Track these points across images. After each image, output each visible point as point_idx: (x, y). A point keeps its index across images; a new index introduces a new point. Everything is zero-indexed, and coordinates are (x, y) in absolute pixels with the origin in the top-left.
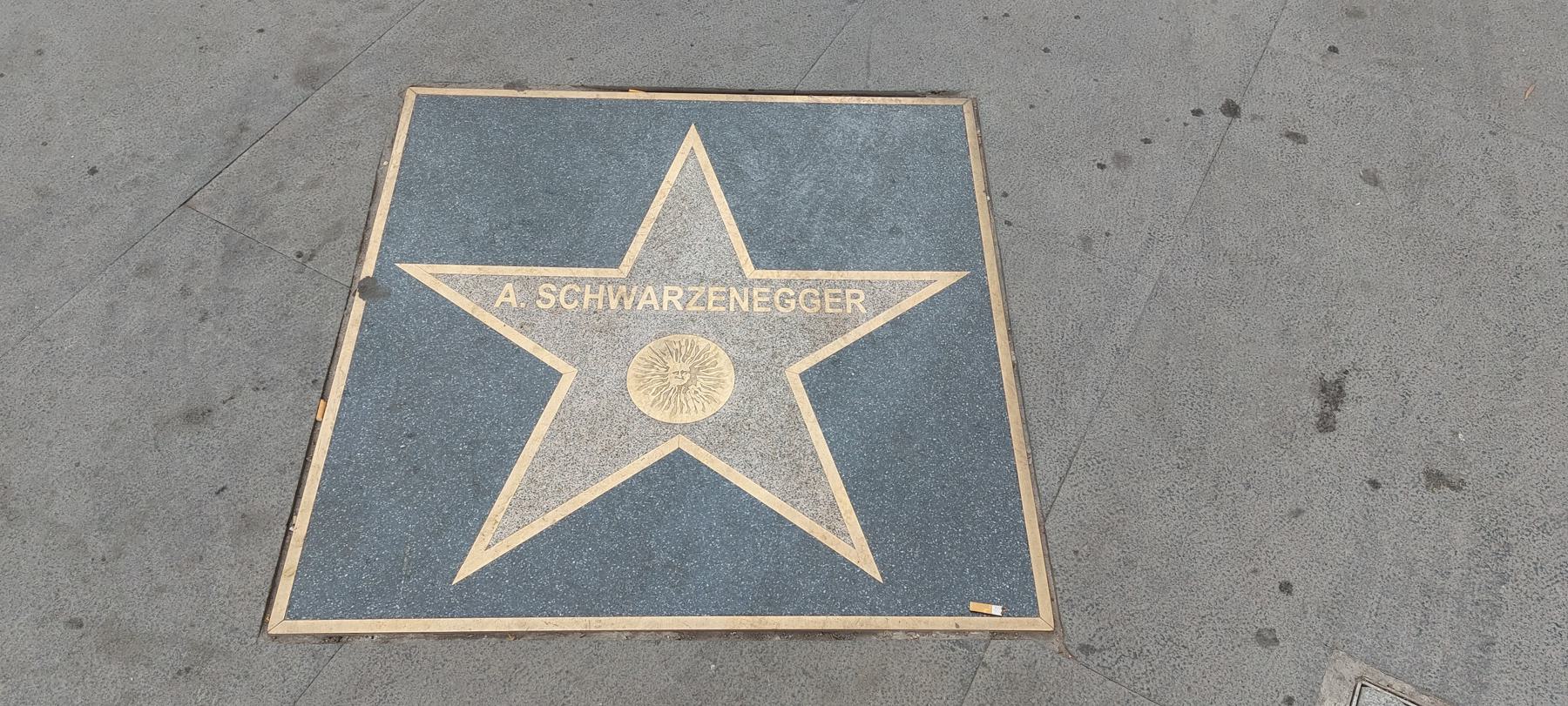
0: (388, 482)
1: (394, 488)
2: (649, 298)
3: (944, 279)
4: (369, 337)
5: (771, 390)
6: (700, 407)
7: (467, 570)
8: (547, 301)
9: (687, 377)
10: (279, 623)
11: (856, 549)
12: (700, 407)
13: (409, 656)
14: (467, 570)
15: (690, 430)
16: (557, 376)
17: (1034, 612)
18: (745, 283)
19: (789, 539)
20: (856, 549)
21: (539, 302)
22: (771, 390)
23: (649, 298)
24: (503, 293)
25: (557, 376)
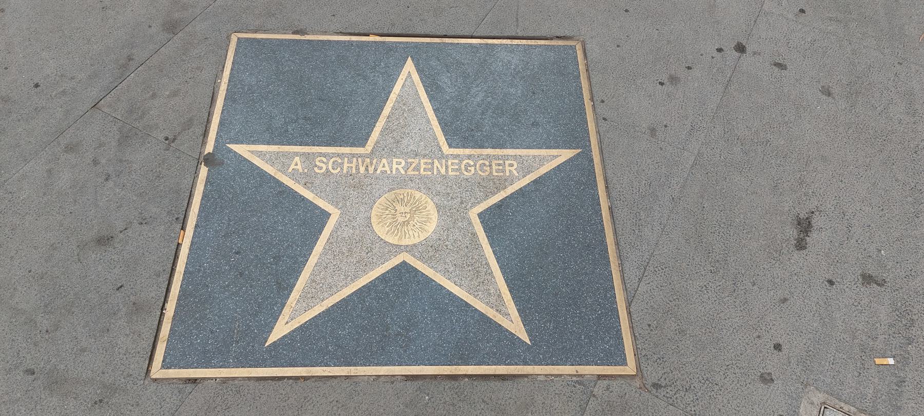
0: (224, 282)
1: (228, 286)
2: (296, 165)
3: (565, 154)
4: (211, 191)
5: (460, 224)
6: (416, 235)
7: (274, 337)
8: (321, 168)
9: (408, 216)
10: (157, 371)
11: (513, 323)
12: (416, 235)
13: (238, 392)
14: (274, 337)
15: (409, 249)
16: (326, 215)
17: (624, 362)
18: (443, 156)
19: (472, 317)
20: (513, 323)
21: (316, 169)
22: (460, 224)
23: (296, 165)
24: (294, 163)
25: (326, 215)
